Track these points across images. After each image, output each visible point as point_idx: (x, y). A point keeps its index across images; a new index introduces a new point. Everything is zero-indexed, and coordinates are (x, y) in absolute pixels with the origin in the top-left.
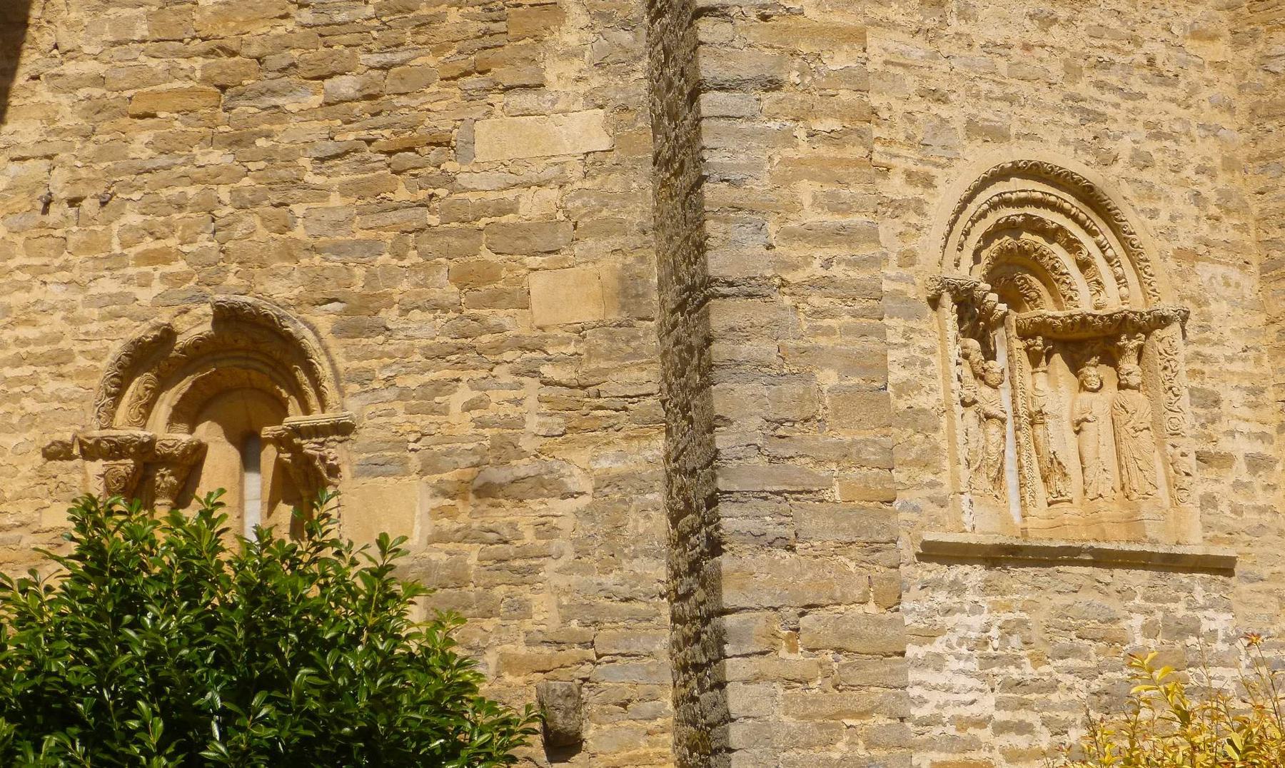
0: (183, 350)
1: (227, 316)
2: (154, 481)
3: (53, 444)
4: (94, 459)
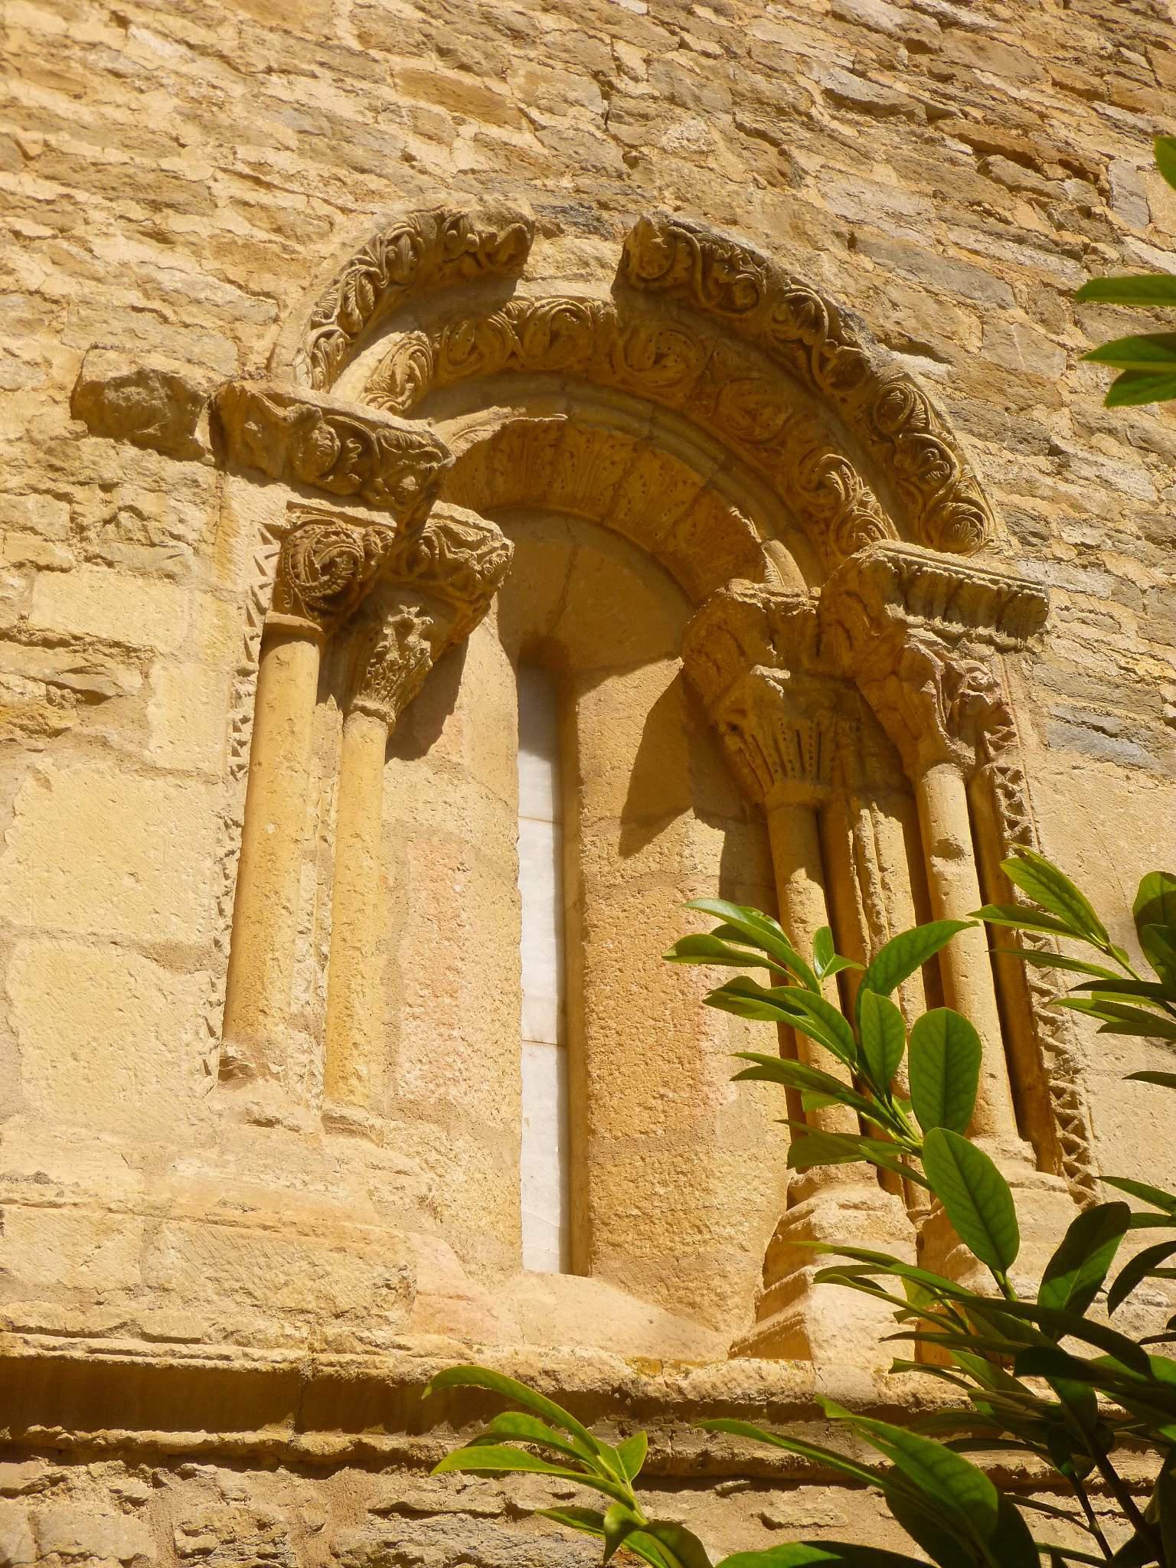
0: (525, 322)
1: (685, 281)
2: (379, 635)
3: (141, 378)
4: (261, 476)
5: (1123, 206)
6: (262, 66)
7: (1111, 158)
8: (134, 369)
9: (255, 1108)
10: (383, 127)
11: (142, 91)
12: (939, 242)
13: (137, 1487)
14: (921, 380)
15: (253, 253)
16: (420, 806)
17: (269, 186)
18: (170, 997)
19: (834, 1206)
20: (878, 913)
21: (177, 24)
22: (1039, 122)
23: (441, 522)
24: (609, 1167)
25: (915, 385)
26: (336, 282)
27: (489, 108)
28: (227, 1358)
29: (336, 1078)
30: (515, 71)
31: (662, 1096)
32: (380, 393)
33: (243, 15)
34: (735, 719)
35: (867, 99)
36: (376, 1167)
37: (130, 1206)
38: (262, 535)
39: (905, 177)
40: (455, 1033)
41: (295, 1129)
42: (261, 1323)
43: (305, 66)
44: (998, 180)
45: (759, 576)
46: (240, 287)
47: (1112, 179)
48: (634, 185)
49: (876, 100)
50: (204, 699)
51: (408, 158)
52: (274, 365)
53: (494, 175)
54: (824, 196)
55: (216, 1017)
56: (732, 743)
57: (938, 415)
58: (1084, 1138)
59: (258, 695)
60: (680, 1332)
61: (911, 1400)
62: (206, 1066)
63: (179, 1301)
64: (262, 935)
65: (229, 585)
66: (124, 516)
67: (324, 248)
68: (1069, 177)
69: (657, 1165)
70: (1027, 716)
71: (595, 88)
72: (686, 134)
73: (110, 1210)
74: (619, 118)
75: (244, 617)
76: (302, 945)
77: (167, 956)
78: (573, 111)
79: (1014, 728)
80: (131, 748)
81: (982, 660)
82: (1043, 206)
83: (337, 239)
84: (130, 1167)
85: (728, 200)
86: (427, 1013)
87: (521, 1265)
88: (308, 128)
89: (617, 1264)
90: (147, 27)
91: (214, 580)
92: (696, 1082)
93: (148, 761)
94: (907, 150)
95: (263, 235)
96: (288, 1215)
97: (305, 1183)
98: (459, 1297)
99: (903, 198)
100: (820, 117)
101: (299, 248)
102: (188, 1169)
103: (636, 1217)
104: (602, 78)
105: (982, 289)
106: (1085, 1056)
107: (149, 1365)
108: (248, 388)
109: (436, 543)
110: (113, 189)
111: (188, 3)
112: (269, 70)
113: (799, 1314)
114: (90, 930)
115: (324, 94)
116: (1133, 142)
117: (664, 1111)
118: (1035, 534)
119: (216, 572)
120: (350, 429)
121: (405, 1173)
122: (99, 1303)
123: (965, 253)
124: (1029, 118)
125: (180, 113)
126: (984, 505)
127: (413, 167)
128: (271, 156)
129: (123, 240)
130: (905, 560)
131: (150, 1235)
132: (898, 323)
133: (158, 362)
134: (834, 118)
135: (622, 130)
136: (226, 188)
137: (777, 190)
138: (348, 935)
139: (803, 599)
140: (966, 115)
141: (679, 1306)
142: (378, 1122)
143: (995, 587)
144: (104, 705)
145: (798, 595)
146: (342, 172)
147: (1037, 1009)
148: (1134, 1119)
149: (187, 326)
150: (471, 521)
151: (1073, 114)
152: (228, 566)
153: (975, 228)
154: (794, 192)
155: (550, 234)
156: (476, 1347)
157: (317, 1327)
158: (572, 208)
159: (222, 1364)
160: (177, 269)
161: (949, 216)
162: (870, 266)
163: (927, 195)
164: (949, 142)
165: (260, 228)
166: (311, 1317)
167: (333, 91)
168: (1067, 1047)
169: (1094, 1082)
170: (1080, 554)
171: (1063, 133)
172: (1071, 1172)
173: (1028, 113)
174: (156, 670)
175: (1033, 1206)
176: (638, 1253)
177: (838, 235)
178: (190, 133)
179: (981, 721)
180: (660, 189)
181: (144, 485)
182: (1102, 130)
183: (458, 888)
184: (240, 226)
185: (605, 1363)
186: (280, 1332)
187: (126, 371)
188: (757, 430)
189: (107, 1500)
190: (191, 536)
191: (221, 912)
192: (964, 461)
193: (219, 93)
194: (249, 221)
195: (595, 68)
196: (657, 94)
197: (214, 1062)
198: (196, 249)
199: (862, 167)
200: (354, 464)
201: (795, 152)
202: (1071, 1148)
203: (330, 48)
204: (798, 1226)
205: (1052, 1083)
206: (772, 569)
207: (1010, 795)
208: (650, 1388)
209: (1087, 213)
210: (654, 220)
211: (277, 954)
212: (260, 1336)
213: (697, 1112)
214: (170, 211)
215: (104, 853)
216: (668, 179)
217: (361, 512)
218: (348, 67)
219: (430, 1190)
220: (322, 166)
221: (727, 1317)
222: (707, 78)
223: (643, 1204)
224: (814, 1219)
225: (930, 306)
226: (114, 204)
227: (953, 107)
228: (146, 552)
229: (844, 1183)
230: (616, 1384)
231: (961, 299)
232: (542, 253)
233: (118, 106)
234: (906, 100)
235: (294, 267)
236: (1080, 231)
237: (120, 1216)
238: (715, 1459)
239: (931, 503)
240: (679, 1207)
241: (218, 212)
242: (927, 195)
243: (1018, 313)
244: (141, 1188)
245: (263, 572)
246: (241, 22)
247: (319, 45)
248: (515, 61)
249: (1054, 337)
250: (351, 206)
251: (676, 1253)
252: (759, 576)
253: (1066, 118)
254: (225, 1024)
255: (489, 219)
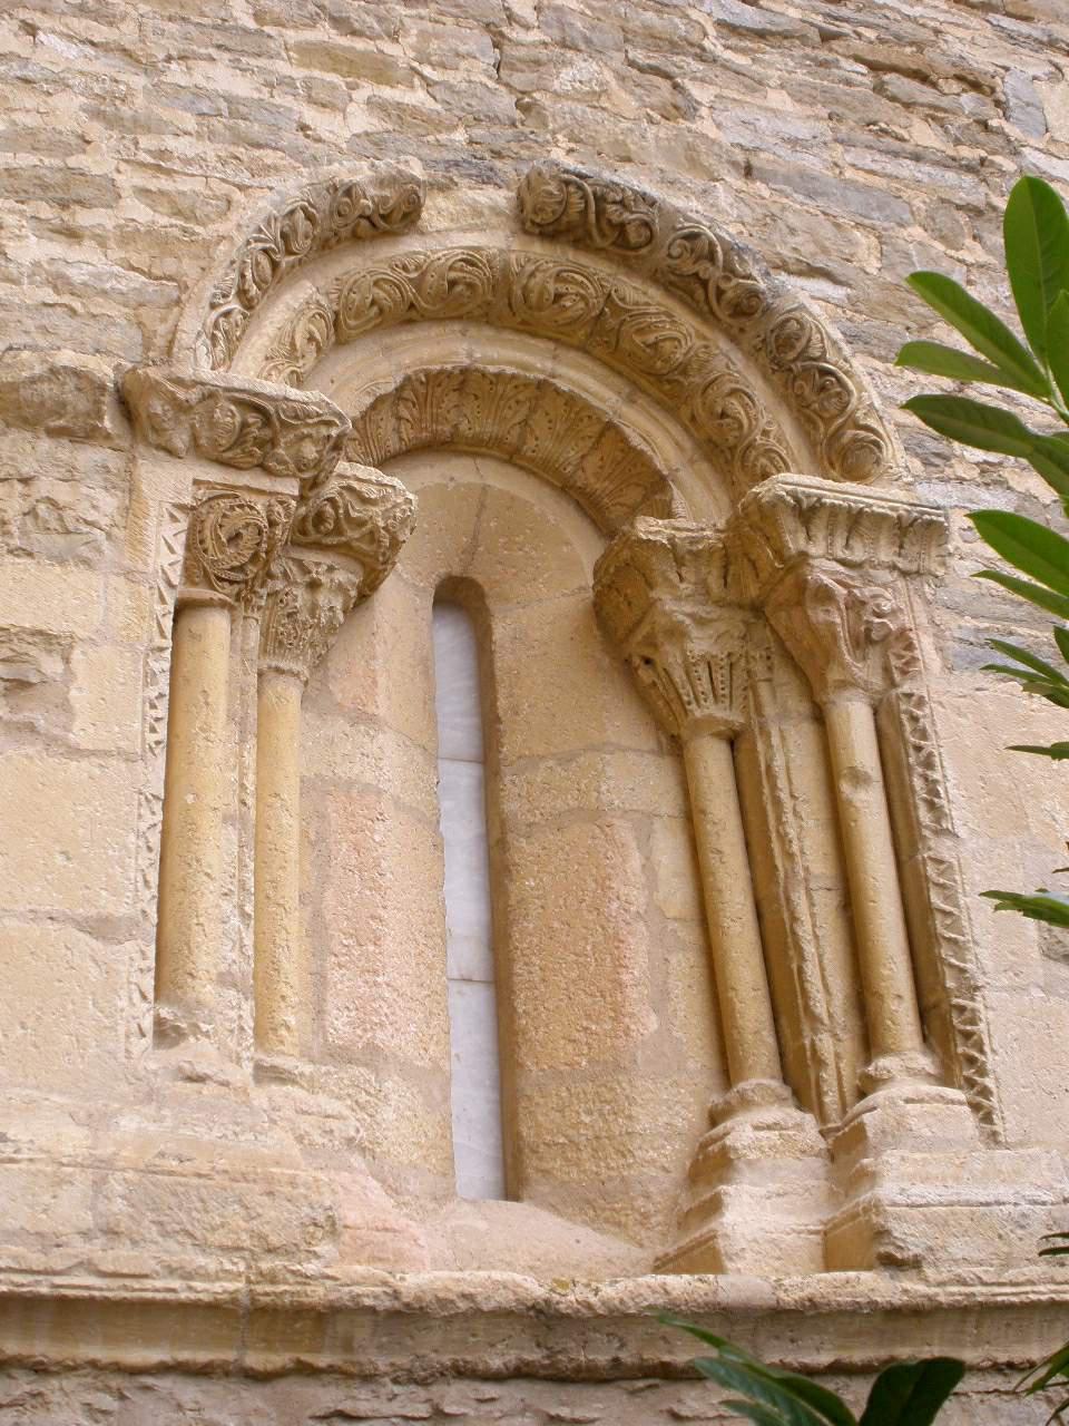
5: (1021, 117)
6: (161, 56)
7: (1007, 69)
8: (46, 367)
9: (186, 1066)
10: (277, 100)
11: (50, 94)
12: (836, 164)
13: (107, 1401)
14: (816, 308)
15: (160, 242)
16: (338, 759)
17: (169, 172)
18: (104, 967)
19: (749, 1128)
20: (791, 842)
21: (80, 25)
22: (934, 38)
23: (344, 483)
24: (538, 1099)
25: (811, 314)
26: (233, 262)
27: (382, 71)
28: (173, 1290)
29: (264, 1031)
30: (407, 32)
31: (586, 1029)
32: (281, 360)
33: (143, 8)
34: (648, 652)
35: (760, 27)
36: (304, 1113)
37: (79, 1160)
38: (172, 516)
39: (799, 101)
40: (379, 979)
41: (225, 1084)
42: (201, 1260)
43: (202, 51)
44: (893, 99)
45: (667, 512)
46: (142, 272)
47: (1008, 91)
48: (527, 130)
49: (768, 26)
50: (122, 680)
51: (303, 128)
52: (175, 350)
53: (386, 136)
54: (719, 126)
55: (148, 983)
56: (645, 675)
57: (834, 343)
58: (982, 1051)
59: (173, 671)
60: (605, 1250)
61: (807, 1303)
62: (140, 1029)
63: (128, 1242)
64: (186, 903)
65: (140, 566)
66: (42, 508)
67: (222, 227)
68: (964, 91)
69: (582, 1096)
70: (931, 640)
71: (487, 40)
72: (578, 77)
73: (63, 1165)
74: (513, 68)
75: (156, 596)
76: (227, 906)
77: (102, 928)
78: (463, 64)
79: (917, 653)
80: (57, 731)
81: (885, 586)
82: (941, 123)
83: (234, 217)
84: (78, 1124)
85: (621, 137)
86: (351, 962)
87: (455, 1194)
88: (205, 111)
89: (546, 1189)
90: (53, 32)
91: (126, 562)
92: (618, 1013)
93: (72, 743)
94: (801, 75)
95: (164, 221)
96: (222, 1164)
97: (235, 1134)
98: (386, 1230)
99: (799, 123)
100: (712, 47)
101: (198, 229)
102: (129, 1123)
103: (563, 1144)
104: (492, 28)
105: (880, 208)
106: (984, 973)
107: (106, 1298)
108: (151, 375)
109: (341, 504)
110: (25, 191)
111: (91, 1)
112: (169, 59)
113: (713, 1231)
114: (29, 907)
115: (223, 78)
116: (1027, 51)
117: (587, 1043)
118: (938, 455)
119: (127, 555)
120: (252, 404)
121: (333, 1117)
122: (58, 1246)
123: (861, 173)
124: (928, 35)
125: (84, 111)
126: (881, 430)
127: (307, 136)
128: (171, 143)
129: (33, 238)
130: (803, 492)
131: (99, 1184)
132: (795, 249)
133: (66, 357)
134: (727, 47)
135: (518, 80)
136: (128, 179)
137: (671, 123)
138: (271, 893)
139: (708, 533)
140: (859, 35)
141: (605, 1226)
142: (308, 1069)
143: (895, 514)
144: (31, 691)
145: (703, 529)
146: (240, 151)
147: (940, 930)
148: (1030, 1031)
149: (94, 316)
150: (373, 478)
151: (967, 28)
152: (139, 547)
153: (871, 147)
154: (688, 124)
155: (444, 188)
156: (398, 1276)
157: (253, 1263)
158: (464, 161)
159: (169, 1296)
160: (85, 262)
161: (845, 138)
162: (766, 193)
163: (822, 119)
164: (844, 63)
165: (161, 213)
166: (247, 1254)
167: (231, 71)
168: (968, 966)
169: (991, 996)
170: (983, 472)
171: (957, 48)
172: (971, 1083)
173: (923, 30)
174: (76, 655)
175: (930, 1120)
176: (566, 1178)
177: (734, 164)
178: (95, 130)
179: (889, 646)
180: (554, 133)
181: (58, 476)
182: (998, 42)
183: (377, 838)
184: (141, 213)
185: (519, 1286)
186: (219, 1267)
187: (38, 370)
188: (659, 364)
189: (79, 1412)
190: (104, 522)
191: (146, 882)
192: (861, 388)
193: (122, 87)
194: (151, 208)
195: (485, 20)
196: (548, 40)
197: (148, 1023)
198: (102, 242)
199: (757, 94)
200: (256, 434)
201: (688, 84)
202: (972, 1061)
203: (226, 29)
204: (714, 1148)
205: (955, 1001)
206: (679, 505)
207: (915, 719)
208: (562, 1306)
209: (985, 126)
210: (544, 169)
211: (201, 920)
212: (202, 1272)
213: (618, 1042)
214: (77, 208)
215: (37, 834)
216: (561, 122)
217: (265, 483)
218: (239, 45)
219: (358, 1131)
220: (220, 146)
221: (651, 1234)
222: (599, 19)
223: (571, 1132)
224: (728, 1141)
225: (827, 231)
226: (24, 207)
227: (846, 28)
228: (60, 540)
229: (759, 1105)
230: (530, 1304)
231: (859, 219)
232: (435, 210)
233: (28, 111)
234: (798, 26)
235: (194, 248)
236: (976, 144)
237: (70, 1170)
238: (626, 1365)
239: (833, 428)
240: (604, 1134)
241: (122, 202)
242: (822, 119)
243: (917, 232)
244: (89, 1142)
245: (172, 551)
246: (142, 16)
247: (215, 27)
248: (407, 21)
249: (952, 253)
250: (247, 182)
251: (602, 1177)
252: (667, 512)
253: (960, 33)
254: (157, 989)
255: (381, 183)
